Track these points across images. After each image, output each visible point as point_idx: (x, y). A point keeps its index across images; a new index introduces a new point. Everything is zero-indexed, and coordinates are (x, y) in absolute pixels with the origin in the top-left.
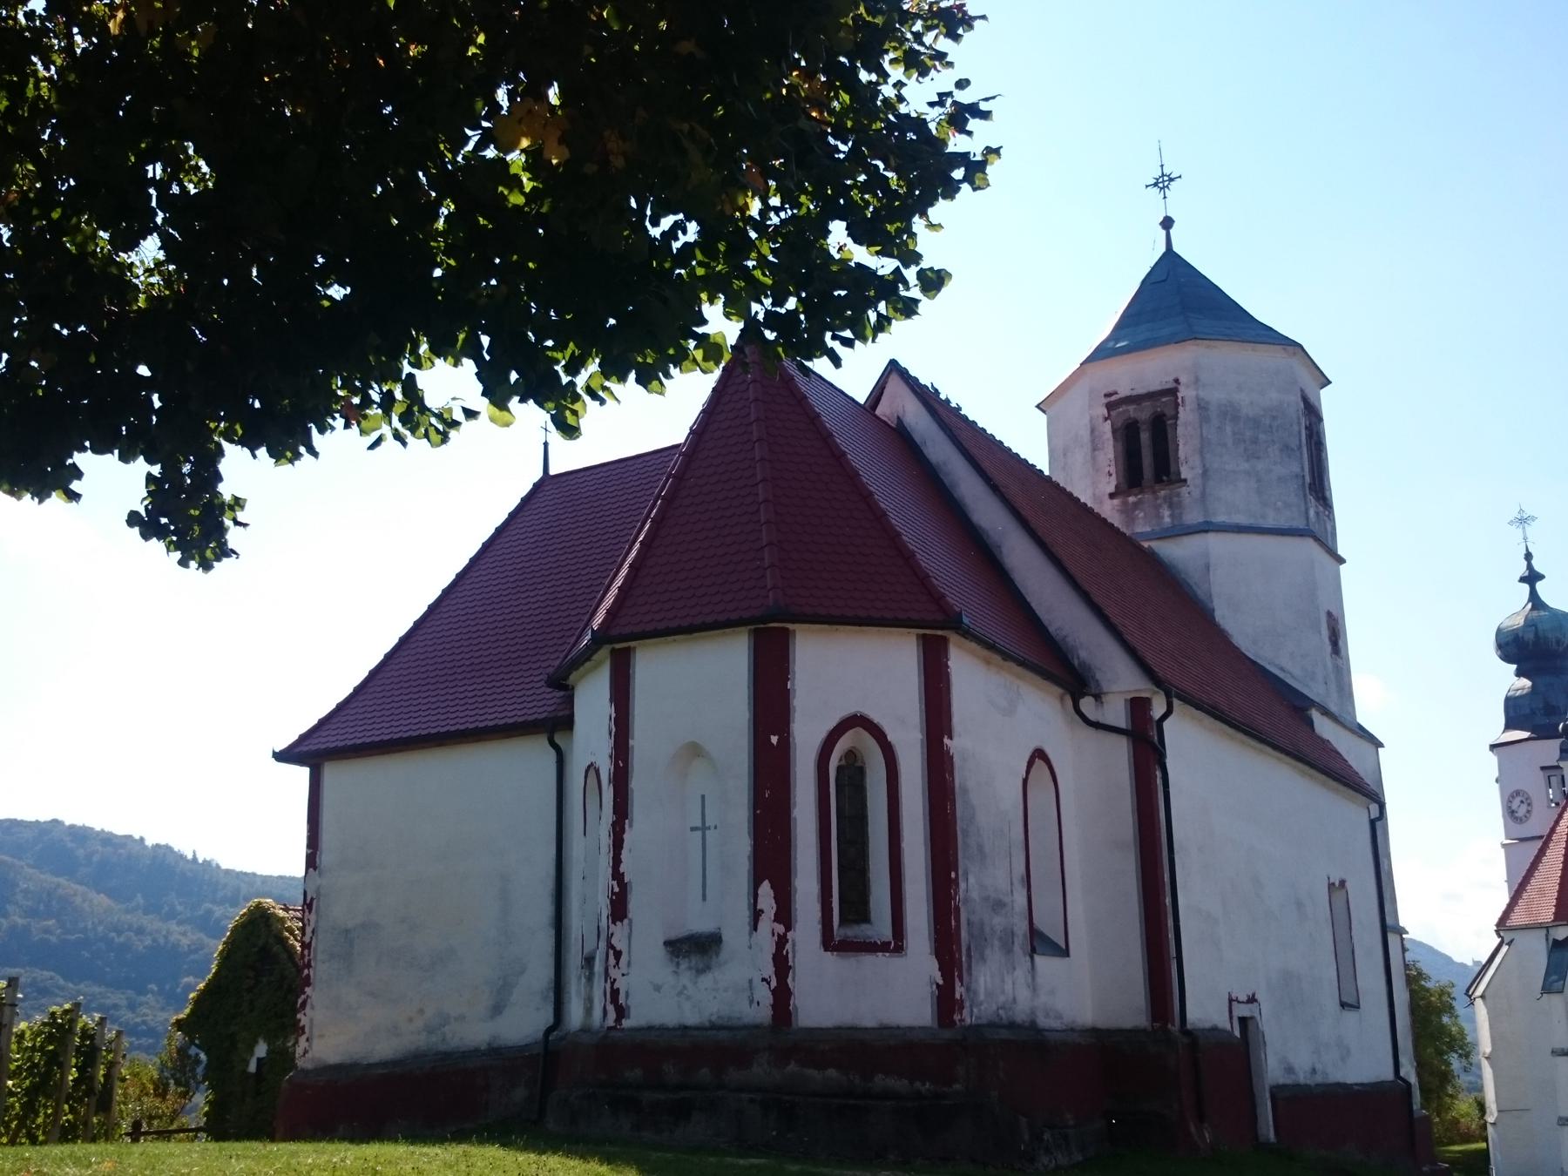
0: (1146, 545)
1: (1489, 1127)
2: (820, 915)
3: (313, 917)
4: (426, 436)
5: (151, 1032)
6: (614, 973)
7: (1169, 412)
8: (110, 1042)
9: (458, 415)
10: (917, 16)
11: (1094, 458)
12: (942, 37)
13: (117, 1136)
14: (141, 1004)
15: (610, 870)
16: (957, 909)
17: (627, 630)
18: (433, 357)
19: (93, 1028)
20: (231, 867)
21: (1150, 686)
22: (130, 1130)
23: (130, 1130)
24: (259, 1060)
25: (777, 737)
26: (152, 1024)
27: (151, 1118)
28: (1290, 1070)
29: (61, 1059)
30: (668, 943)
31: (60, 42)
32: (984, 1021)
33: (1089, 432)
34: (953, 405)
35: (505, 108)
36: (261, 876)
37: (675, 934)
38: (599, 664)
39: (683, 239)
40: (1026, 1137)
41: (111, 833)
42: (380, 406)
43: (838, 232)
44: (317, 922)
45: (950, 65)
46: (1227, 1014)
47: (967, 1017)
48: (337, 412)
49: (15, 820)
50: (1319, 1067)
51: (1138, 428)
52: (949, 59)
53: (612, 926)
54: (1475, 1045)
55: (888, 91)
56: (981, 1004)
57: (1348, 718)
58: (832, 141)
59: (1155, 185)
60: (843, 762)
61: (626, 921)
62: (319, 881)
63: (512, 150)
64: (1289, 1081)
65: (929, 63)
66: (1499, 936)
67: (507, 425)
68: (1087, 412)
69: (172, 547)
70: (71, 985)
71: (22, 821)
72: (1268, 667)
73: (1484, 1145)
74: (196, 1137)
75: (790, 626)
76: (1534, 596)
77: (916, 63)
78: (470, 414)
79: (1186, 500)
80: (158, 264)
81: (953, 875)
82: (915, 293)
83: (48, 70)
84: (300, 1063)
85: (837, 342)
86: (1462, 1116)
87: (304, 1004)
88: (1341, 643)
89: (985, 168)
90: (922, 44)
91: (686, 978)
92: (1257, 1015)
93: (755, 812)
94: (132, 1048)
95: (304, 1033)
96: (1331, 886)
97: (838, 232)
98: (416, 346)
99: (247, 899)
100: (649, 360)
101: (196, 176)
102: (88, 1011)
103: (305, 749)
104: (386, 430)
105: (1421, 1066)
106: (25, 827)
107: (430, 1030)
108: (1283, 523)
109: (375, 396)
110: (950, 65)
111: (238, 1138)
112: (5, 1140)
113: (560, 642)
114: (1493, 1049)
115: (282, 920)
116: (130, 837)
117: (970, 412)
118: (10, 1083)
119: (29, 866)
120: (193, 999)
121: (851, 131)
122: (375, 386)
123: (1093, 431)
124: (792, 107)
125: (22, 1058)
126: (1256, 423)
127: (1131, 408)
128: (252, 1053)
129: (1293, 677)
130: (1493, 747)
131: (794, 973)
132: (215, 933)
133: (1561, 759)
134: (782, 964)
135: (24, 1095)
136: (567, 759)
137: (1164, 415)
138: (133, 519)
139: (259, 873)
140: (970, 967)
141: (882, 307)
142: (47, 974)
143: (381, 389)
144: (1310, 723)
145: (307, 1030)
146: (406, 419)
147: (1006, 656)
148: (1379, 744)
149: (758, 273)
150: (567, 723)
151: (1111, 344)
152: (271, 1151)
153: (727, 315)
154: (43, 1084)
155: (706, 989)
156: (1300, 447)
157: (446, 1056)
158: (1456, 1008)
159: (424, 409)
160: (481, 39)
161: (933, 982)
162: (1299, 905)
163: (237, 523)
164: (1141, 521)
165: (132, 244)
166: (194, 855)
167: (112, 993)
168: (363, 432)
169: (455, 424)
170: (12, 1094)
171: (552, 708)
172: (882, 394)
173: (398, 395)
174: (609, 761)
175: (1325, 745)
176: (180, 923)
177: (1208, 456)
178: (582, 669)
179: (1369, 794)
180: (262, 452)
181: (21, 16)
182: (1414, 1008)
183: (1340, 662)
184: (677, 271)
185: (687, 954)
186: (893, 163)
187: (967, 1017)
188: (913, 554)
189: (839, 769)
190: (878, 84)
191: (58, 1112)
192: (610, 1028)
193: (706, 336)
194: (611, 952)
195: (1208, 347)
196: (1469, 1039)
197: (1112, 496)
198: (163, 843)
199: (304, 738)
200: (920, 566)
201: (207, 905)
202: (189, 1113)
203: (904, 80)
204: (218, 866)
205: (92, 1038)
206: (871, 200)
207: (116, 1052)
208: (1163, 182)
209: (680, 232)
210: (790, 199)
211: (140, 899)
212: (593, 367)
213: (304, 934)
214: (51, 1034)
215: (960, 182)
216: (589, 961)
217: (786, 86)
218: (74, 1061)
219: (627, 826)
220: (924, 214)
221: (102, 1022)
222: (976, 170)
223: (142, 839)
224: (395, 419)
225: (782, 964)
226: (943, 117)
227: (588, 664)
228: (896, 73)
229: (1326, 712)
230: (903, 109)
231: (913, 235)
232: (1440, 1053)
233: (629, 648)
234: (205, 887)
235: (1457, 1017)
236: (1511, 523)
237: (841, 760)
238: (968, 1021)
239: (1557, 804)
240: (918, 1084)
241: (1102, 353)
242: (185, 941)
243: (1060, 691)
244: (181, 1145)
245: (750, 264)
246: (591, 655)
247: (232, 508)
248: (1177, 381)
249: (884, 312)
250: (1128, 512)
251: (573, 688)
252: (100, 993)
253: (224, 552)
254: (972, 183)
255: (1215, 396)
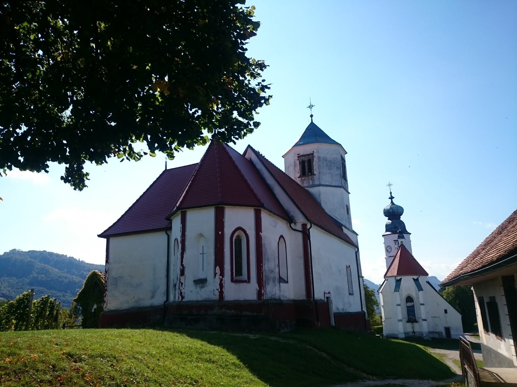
0: (306, 189)
1: (383, 322)
2: (230, 274)
3: (107, 275)
4: (134, 159)
5: (68, 302)
6: (181, 288)
7: (312, 159)
8: (57, 305)
9: (142, 154)
10: (253, 65)
11: (295, 169)
12: (259, 70)
13: (59, 328)
14: (66, 295)
15: (180, 264)
16: (263, 272)
17: (185, 207)
18: (136, 140)
19: (53, 301)
20: (88, 263)
21: (307, 221)
22: (62, 326)
23: (62, 326)
24: (95, 309)
25: (221, 232)
26: (69, 300)
27: (68, 323)
28: (338, 309)
29: (45, 309)
30: (194, 281)
31: (46, 62)
32: (268, 298)
33: (294, 163)
34: (263, 155)
35: (154, 81)
36: (95, 265)
37: (196, 279)
38: (178, 214)
39: (197, 114)
40: (278, 325)
41: (59, 254)
42: (123, 151)
43: (235, 114)
44: (108, 276)
45: (261, 76)
46: (324, 296)
47: (265, 298)
48: (112, 152)
49: (34, 251)
50: (344, 308)
51: (305, 162)
52: (261, 75)
53: (181, 277)
54: (380, 303)
55: (246, 82)
56: (268, 294)
57: (350, 228)
58: (233, 93)
59: (309, 107)
60: (236, 238)
61: (184, 276)
62: (109, 266)
63: (156, 92)
64: (338, 312)
65: (256, 76)
66: (385, 278)
67: (155, 156)
68: (293, 158)
69: (72, 185)
70: (48, 291)
71: (36, 251)
72: (333, 217)
73: (382, 326)
74: (79, 327)
75: (224, 206)
76: (392, 202)
77: (254, 76)
78: (145, 154)
79: (315, 179)
80: (70, 116)
81: (262, 264)
82: (253, 127)
83: (43, 69)
84: (105, 310)
85: (235, 139)
86: (377, 320)
87: (105, 295)
88: (349, 212)
89: (269, 100)
90: (255, 71)
91: (198, 289)
92: (330, 296)
93: (215, 249)
94: (63, 306)
95: (105, 302)
96: (347, 267)
97: (235, 114)
98: (132, 137)
99: (92, 270)
100: (189, 142)
101: (80, 95)
102: (52, 297)
103: (106, 234)
104: (124, 157)
105: (367, 308)
106: (37, 252)
107: (136, 302)
108: (337, 185)
109: (122, 149)
110: (261, 76)
111: (89, 328)
112: (30, 329)
113: (169, 209)
114: (384, 304)
115: (100, 275)
116: (63, 255)
117: (267, 157)
118: (32, 315)
119: (38, 262)
120: (78, 294)
121: (238, 90)
122: (122, 147)
123: (295, 162)
124: (224, 83)
125: (35, 309)
126: (331, 162)
127: (303, 158)
128: (93, 307)
129: (339, 219)
130: (383, 236)
131: (224, 288)
132: (84, 278)
133: (398, 239)
134: (221, 285)
135: (35, 318)
136: (170, 237)
137: (311, 159)
138: (62, 178)
139: (95, 264)
140: (265, 286)
141: (245, 131)
142: (42, 288)
143: (123, 147)
144: (342, 230)
145: (106, 302)
146: (129, 155)
147: (274, 214)
148: (357, 235)
149: (216, 123)
150: (170, 228)
151: (299, 143)
152: (96, 331)
153: (208, 132)
154: (40, 315)
155: (203, 292)
156: (340, 168)
157: (140, 308)
158: (375, 295)
159: (134, 152)
160: (150, 65)
161: (257, 289)
162: (340, 271)
163: (87, 179)
164: (305, 184)
165: (62, 111)
166: (79, 259)
167: (59, 293)
168: (119, 158)
169: (142, 156)
170: (32, 318)
171: (167, 225)
172: (246, 153)
173: (127, 149)
174: (180, 238)
175: (346, 235)
176: (75, 276)
177: (320, 169)
178: (174, 216)
179: (355, 246)
180: (94, 162)
181: (36, 55)
182: (366, 295)
183: (349, 216)
184: (196, 121)
185: (199, 284)
186: (247, 98)
187: (265, 298)
188: (253, 190)
189: (235, 240)
190: (244, 80)
191: (44, 322)
192: (180, 301)
193: (203, 137)
194: (180, 283)
195: (320, 144)
196: (378, 302)
197: (299, 177)
198: (71, 256)
199: (105, 231)
200: (255, 193)
201: (82, 271)
202: (77, 322)
203: (250, 79)
204: (85, 262)
205: (53, 304)
206: (243, 107)
207: (59, 307)
208: (311, 107)
209: (197, 112)
210: (223, 106)
211: (66, 270)
212: (176, 144)
213: (105, 279)
214: (42, 303)
215: (263, 103)
216: (175, 285)
217: (222, 79)
218: (48, 309)
219: (184, 253)
220: (255, 110)
221: (55, 300)
222: (267, 100)
223: (66, 255)
224: (127, 155)
225: (221, 285)
226: (259, 88)
227: (176, 214)
228: (249, 78)
229: (346, 227)
230: (250, 86)
231: (252, 115)
232: (372, 305)
233: (185, 211)
234: (82, 267)
235: (375, 297)
236: (387, 185)
237: (236, 238)
238: (265, 298)
239: (397, 249)
240: (253, 313)
241: (297, 145)
242: (77, 280)
243: (286, 222)
244: (74, 330)
245: (214, 121)
246: (176, 212)
247: (86, 175)
248: (313, 152)
249: (245, 132)
250: (302, 181)
251: (172, 220)
252: (56, 293)
253: (84, 186)
254: (266, 104)
255: (322, 155)
